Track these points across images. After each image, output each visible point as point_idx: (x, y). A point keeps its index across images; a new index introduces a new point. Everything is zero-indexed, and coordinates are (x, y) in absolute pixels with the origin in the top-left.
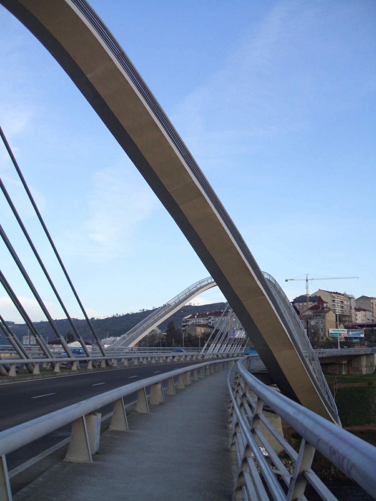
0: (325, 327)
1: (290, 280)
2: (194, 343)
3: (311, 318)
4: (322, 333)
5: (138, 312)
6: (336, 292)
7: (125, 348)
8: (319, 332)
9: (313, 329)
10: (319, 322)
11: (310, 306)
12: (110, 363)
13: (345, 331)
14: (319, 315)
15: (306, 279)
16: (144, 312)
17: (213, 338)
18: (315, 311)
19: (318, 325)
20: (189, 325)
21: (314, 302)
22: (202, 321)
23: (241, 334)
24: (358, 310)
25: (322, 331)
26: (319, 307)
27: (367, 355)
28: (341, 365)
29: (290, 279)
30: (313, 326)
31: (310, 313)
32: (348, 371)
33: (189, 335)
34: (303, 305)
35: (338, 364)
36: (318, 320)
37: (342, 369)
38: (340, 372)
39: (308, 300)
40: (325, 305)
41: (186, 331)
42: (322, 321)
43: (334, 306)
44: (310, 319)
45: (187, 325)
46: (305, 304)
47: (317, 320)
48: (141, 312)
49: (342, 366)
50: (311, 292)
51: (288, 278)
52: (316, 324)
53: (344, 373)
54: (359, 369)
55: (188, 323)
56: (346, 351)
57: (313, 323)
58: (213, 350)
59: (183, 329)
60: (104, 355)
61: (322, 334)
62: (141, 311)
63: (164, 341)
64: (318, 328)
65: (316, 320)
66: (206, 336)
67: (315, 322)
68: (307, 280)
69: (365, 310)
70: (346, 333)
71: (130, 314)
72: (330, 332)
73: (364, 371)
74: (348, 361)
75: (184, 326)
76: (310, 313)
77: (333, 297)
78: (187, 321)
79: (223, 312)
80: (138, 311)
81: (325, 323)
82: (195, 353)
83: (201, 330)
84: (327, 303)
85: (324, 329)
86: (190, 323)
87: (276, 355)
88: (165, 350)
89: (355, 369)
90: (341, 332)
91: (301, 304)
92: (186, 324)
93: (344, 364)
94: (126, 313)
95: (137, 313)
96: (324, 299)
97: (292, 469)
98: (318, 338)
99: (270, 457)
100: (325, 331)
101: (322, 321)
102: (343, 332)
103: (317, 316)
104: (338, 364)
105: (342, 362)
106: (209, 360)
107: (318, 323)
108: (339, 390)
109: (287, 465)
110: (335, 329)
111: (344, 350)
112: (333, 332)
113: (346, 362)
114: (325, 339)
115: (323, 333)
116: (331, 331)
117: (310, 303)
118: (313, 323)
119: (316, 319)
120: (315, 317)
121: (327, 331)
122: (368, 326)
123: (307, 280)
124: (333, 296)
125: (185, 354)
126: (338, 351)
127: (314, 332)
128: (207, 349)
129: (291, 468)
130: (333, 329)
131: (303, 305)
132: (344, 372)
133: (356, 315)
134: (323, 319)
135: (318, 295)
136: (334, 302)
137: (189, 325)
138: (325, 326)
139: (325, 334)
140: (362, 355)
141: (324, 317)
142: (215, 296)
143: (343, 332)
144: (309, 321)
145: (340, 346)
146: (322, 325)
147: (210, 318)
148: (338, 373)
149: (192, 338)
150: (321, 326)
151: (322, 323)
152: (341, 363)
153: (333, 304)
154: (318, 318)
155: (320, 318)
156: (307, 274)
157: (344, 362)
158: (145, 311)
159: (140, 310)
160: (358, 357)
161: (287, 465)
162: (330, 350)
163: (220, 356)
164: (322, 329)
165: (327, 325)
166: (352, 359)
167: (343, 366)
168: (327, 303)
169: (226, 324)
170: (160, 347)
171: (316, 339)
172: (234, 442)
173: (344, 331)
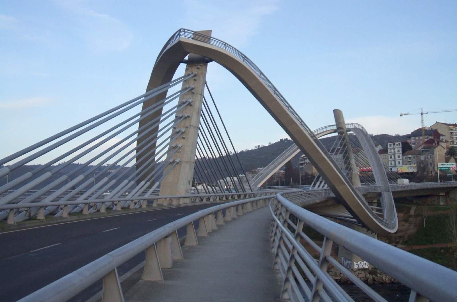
0: (434, 161)
1: (404, 114)
4: (431, 167)
5: (253, 149)
6: (454, 124)
7: (256, 188)
8: (428, 166)
9: (423, 163)
10: (428, 157)
13: (454, 165)
14: (428, 151)
15: (421, 113)
16: (260, 148)
19: (427, 160)
20: (306, 163)
21: (430, 135)
25: (431, 165)
26: (434, 141)
28: (439, 196)
29: (405, 113)
30: (422, 161)
32: (447, 202)
33: (306, 173)
34: (419, 139)
35: (437, 196)
36: (427, 155)
37: (440, 200)
38: (438, 203)
39: (423, 133)
40: (441, 137)
41: (303, 170)
42: (431, 156)
43: (452, 139)
44: (420, 154)
45: (304, 163)
46: (421, 138)
47: (426, 155)
48: (256, 148)
49: (440, 197)
50: (428, 124)
51: (403, 113)
52: (425, 160)
53: (441, 204)
55: (305, 160)
57: (422, 158)
59: (301, 167)
60: (252, 192)
61: (431, 168)
62: (256, 147)
63: (283, 180)
64: (427, 163)
65: (425, 155)
67: (424, 157)
68: (422, 114)
70: (455, 167)
71: (245, 151)
72: (439, 166)
74: (445, 193)
75: (302, 164)
77: (451, 129)
78: (304, 159)
79: (340, 148)
80: (253, 148)
81: (434, 158)
84: (444, 136)
85: (433, 164)
87: (337, 188)
88: (279, 188)
89: (453, 200)
90: (450, 166)
91: (417, 138)
92: (303, 162)
93: (442, 195)
94: (241, 151)
95: (252, 150)
96: (440, 132)
97: (385, 276)
98: (428, 172)
100: (434, 166)
101: (431, 156)
102: (452, 166)
103: (426, 151)
104: (437, 196)
105: (440, 194)
107: (427, 158)
108: (428, 217)
109: (381, 274)
110: (446, 163)
112: (441, 166)
113: (444, 194)
114: (434, 173)
115: (432, 167)
116: (440, 165)
117: (427, 136)
118: (422, 158)
119: (425, 154)
120: (424, 152)
121: (436, 165)
123: (422, 114)
124: (451, 128)
127: (424, 167)
128: (314, 187)
129: (384, 275)
130: (442, 164)
131: (419, 139)
132: (442, 203)
134: (431, 154)
135: (434, 129)
136: (452, 134)
137: (306, 163)
138: (433, 161)
141: (432, 153)
143: (452, 166)
145: (440, 180)
146: (431, 159)
148: (436, 203)
149: (309, 176)
150: (430, 161)
151: (431, 158)
152: (439, 195)
153: (451, 137)
154: (427, 153)
155: (429, 153)
156: (422, 108)
157: (441, 194)
158: (260, 147)
159: (255, 147)
161: (381, 274)
164: (431, 163)
165: (437, 159)
167: (441, 197)
168: (444, 136)
169: (341, 161)
170: (272, 186)
171: (425, 173)
173: (452, 165)
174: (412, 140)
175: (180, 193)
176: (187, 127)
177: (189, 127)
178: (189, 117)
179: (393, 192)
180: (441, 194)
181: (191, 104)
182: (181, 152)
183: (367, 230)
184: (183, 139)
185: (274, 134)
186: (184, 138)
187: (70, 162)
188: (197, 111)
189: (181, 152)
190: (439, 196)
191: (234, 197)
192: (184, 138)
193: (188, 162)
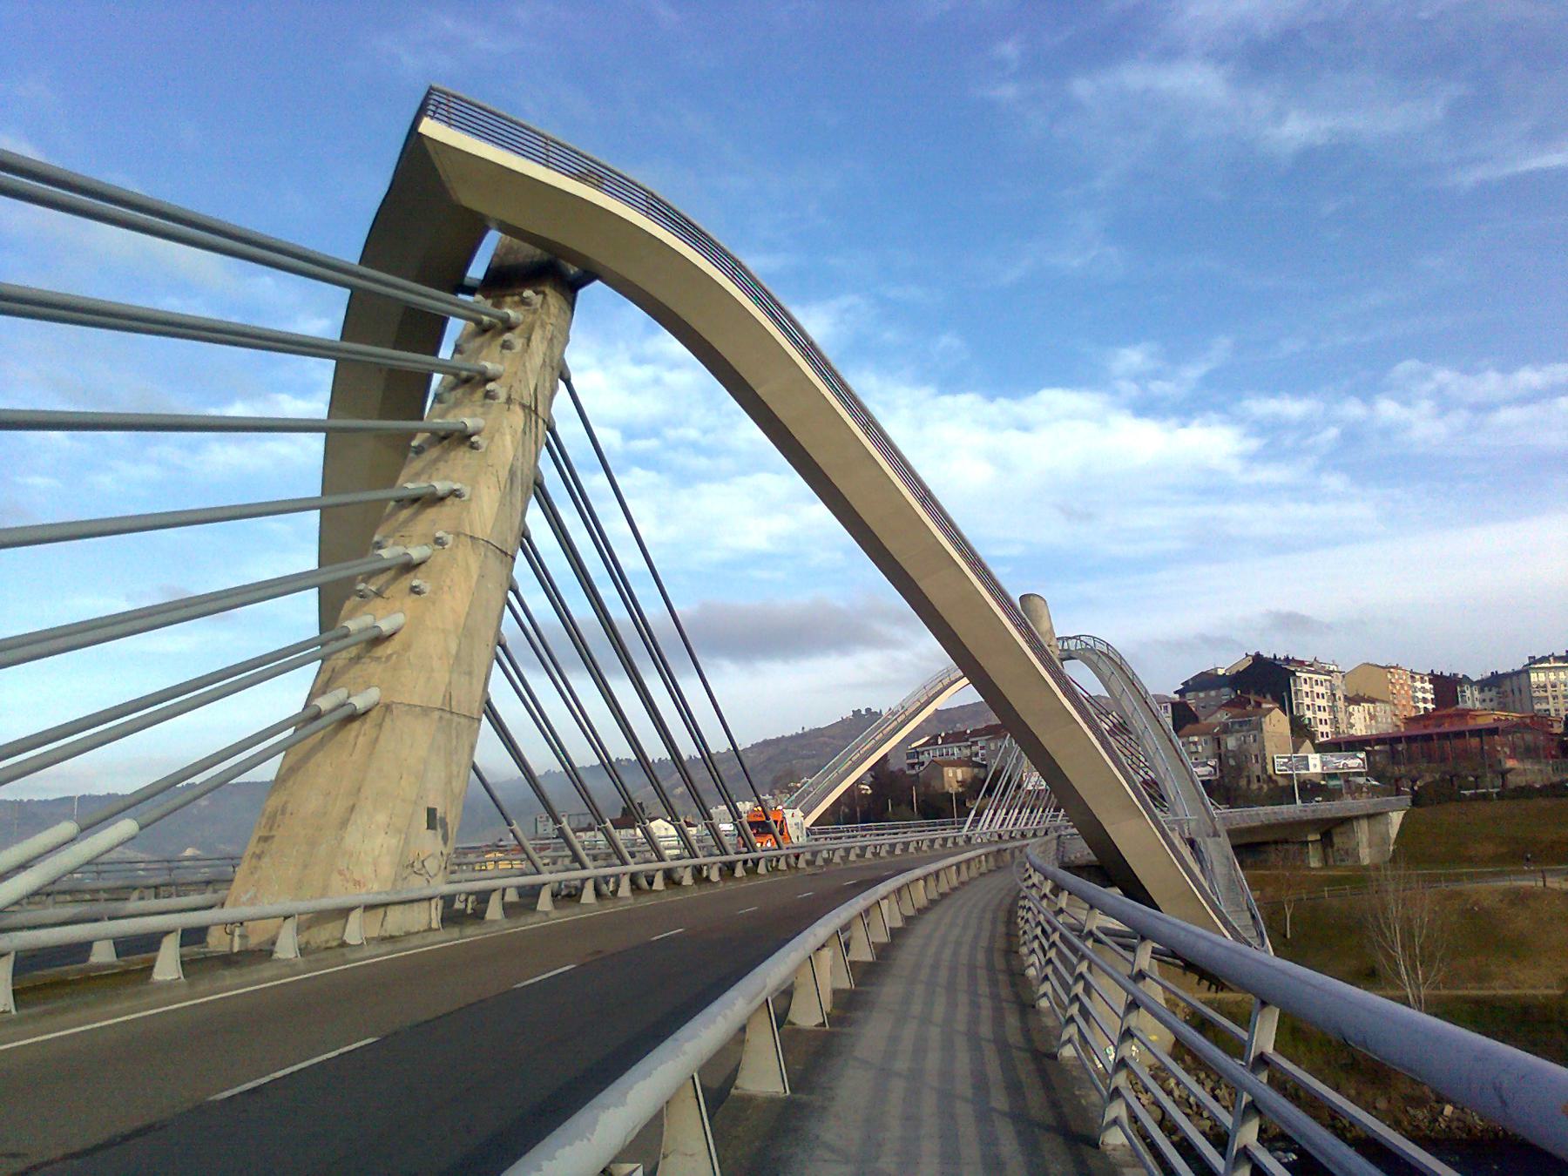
2: (938, 808)
3: (1226, 729)
9: (1234, 757)
11: (1225, 699)
12: (676, 876)
17: (990, 791)
18: (1237, 711)
22: (956, 751)
23: (1034, 781)
24: (1353, 700)
27: (1369, 816)
31: (1223, 716)
52: (1240, 747)
54: (1353, 853)
56: (1322, 808)
58: (991, 822)
61: (1256, 769)
66: (972, 788)
69: (1372, 701)
73: (1366, 856)
76: (1223, 716)
82: (949, 833)
83: (955, 774)
85: (1262, 758)
86: (925, 758)
91: (1202, 695)
99: (1289, 1132)
106: (982, 845)
111: (1311, 806)
118: (1231, 743)
121: (1269, 761)
122: (1379, 740)
125: (916, 835)
126: (1296, 809)
128: (976, 822)
133: (1351, 714)
139: (1264, 769)
140: (1357, 818)
142: (964, 694)
144: (1222, 737)
147: (975, 743)
150: (1254, 749)
160: (1346, 821)
162: (1276, 808)
163: (1006, 837)
166: (1329, 829)
171: (1243, 782)
172: (262, 844)
174: (1191, 700)
175: (357, 883)
176: (439, 542)
177: (450, 538)
178: (455, 494)
179: (1230, 833)
180: (1311, 838)
181: (474, 439)
182: (389, 657)
183: (1196, 978)
184: (415, 596)
185: (889, 673)
186: (415, 591)
187: (222, 779)
188: (504, 474)
189: (389, 657)
190: (1307, 843)
191: (705, 874)
192: (415, 591)
193: (426, 711)
